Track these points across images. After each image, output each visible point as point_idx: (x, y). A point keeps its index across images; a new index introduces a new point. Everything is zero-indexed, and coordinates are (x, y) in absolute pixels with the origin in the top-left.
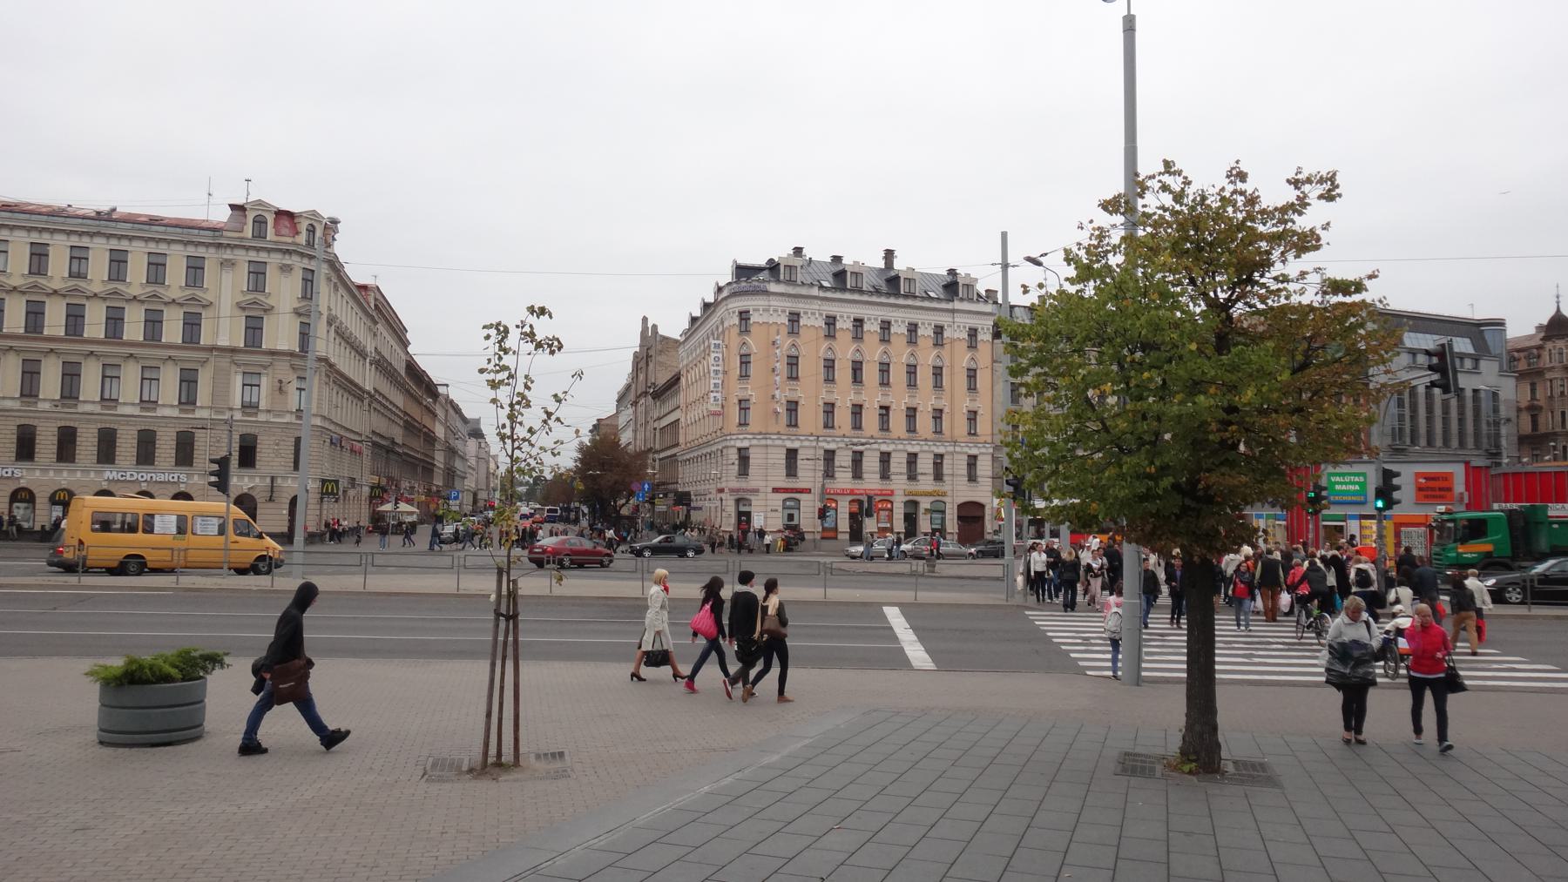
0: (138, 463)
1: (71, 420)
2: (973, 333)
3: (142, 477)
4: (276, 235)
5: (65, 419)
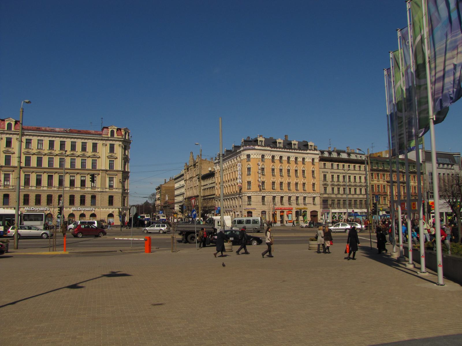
0: (36, 204)
1: (39, 192)
2: (313, 159)
3: (82, 209)
4: (117, 136)
5: (38, 192)
